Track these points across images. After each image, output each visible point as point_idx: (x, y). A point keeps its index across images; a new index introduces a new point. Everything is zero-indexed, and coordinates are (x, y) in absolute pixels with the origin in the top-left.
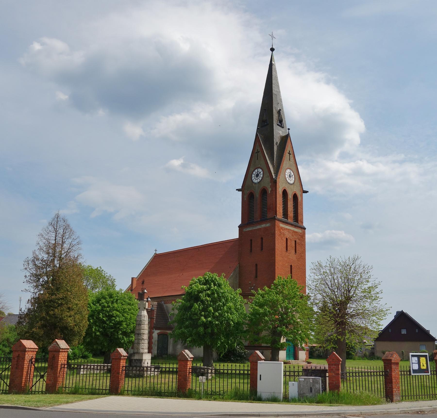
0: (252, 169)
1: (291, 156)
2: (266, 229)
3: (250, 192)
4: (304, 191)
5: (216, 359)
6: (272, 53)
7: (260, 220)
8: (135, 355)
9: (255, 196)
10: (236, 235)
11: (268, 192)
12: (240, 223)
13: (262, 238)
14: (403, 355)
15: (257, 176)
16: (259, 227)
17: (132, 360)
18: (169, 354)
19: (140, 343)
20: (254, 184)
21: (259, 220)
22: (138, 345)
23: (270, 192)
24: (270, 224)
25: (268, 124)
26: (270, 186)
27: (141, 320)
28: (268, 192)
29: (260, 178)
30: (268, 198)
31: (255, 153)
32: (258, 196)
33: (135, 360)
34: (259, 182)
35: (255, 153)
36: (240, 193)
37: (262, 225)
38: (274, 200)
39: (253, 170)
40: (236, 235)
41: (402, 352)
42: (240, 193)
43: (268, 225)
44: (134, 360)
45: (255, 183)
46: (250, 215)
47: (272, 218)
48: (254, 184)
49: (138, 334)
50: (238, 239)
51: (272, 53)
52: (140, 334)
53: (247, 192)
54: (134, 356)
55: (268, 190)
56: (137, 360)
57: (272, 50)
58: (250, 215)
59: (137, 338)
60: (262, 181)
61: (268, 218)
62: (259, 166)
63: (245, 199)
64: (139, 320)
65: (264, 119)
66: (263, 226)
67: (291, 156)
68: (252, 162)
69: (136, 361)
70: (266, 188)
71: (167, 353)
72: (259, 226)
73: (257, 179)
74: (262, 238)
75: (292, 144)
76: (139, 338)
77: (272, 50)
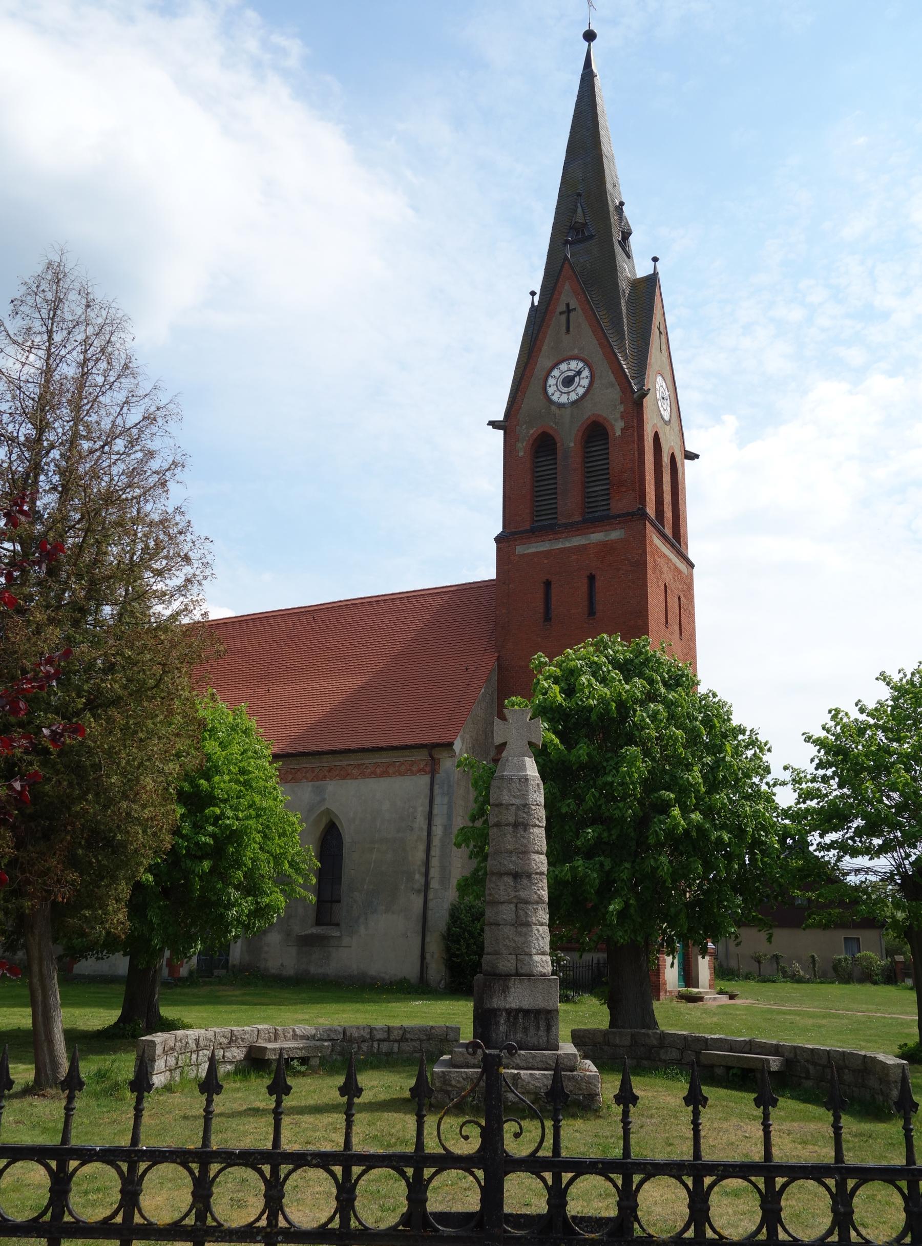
0: (543, 362)
1: (663, 337)
2: (607, 548)
3: (540, 432)
4: (689, 454)
5: (442, 985)
6: (589, 45)
7: (580, 519)
8: (511, 984)
9: (558, 445)
10: (487, 571)
11: (610, 433)
12: (498, 529)
13: (592, 578)
14: (814, 967)
15: (568, 382)
16: (577, 541)
17: (494, 1012)
18: (234, 966)
19: (528, 925)
20: (553, 408)
21: (578, 518)
22: (520, 934)
23: (618, 433)
24: (623, 531)
25: (591, 237)
26: (618, 415)
27: (526, 805)
28: (613, 430)
29: (581, 391)
30: (611, 450)
31: (557, 313)
32: (572, 445)
33: (514, 1014)
34: (574, 403)
35: (557, 313)
36: (500, 434)
37: (592, 535)
38: (636, 458)
39: (550, 364)
40: (487, 571)
41: (813, 957)
42: (500, 434)
43: (615, 535)
44: (509, 1012)
45: (561, 406)
46: (537, 504)
47: (632, 514)
48: (553, 408)
49: (516, 876)
50: (494, 583)
51: (589, 45)
52: (529, 876)
53: (527, 433)
54: (505, 990)
55: (612, 426)
56: (527, 1012)
57: (590, 36)
58: (537, 504)
59: (512, 894)
60: (588, 397)
61: (613, 512)
62: (576, 351)
63: (521, 454)
64: (517, 802)
65: (579, 218)
66: (597, 537)
67: (663, 337)
68: (546, 341)
69: (516, 1018)
70: (605, 419)
71: (227, 961)
72: (578, 538)
73: (568, 393)
74: (592, 578)
75: (662, 304)
76: (523, 894)
77: (590, 36)
